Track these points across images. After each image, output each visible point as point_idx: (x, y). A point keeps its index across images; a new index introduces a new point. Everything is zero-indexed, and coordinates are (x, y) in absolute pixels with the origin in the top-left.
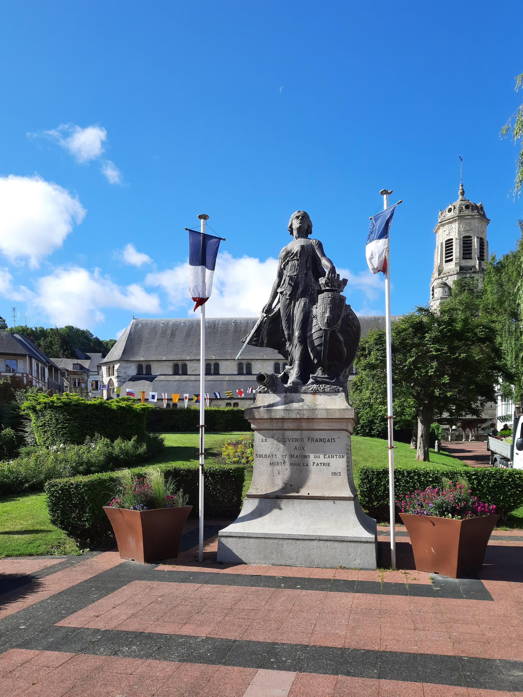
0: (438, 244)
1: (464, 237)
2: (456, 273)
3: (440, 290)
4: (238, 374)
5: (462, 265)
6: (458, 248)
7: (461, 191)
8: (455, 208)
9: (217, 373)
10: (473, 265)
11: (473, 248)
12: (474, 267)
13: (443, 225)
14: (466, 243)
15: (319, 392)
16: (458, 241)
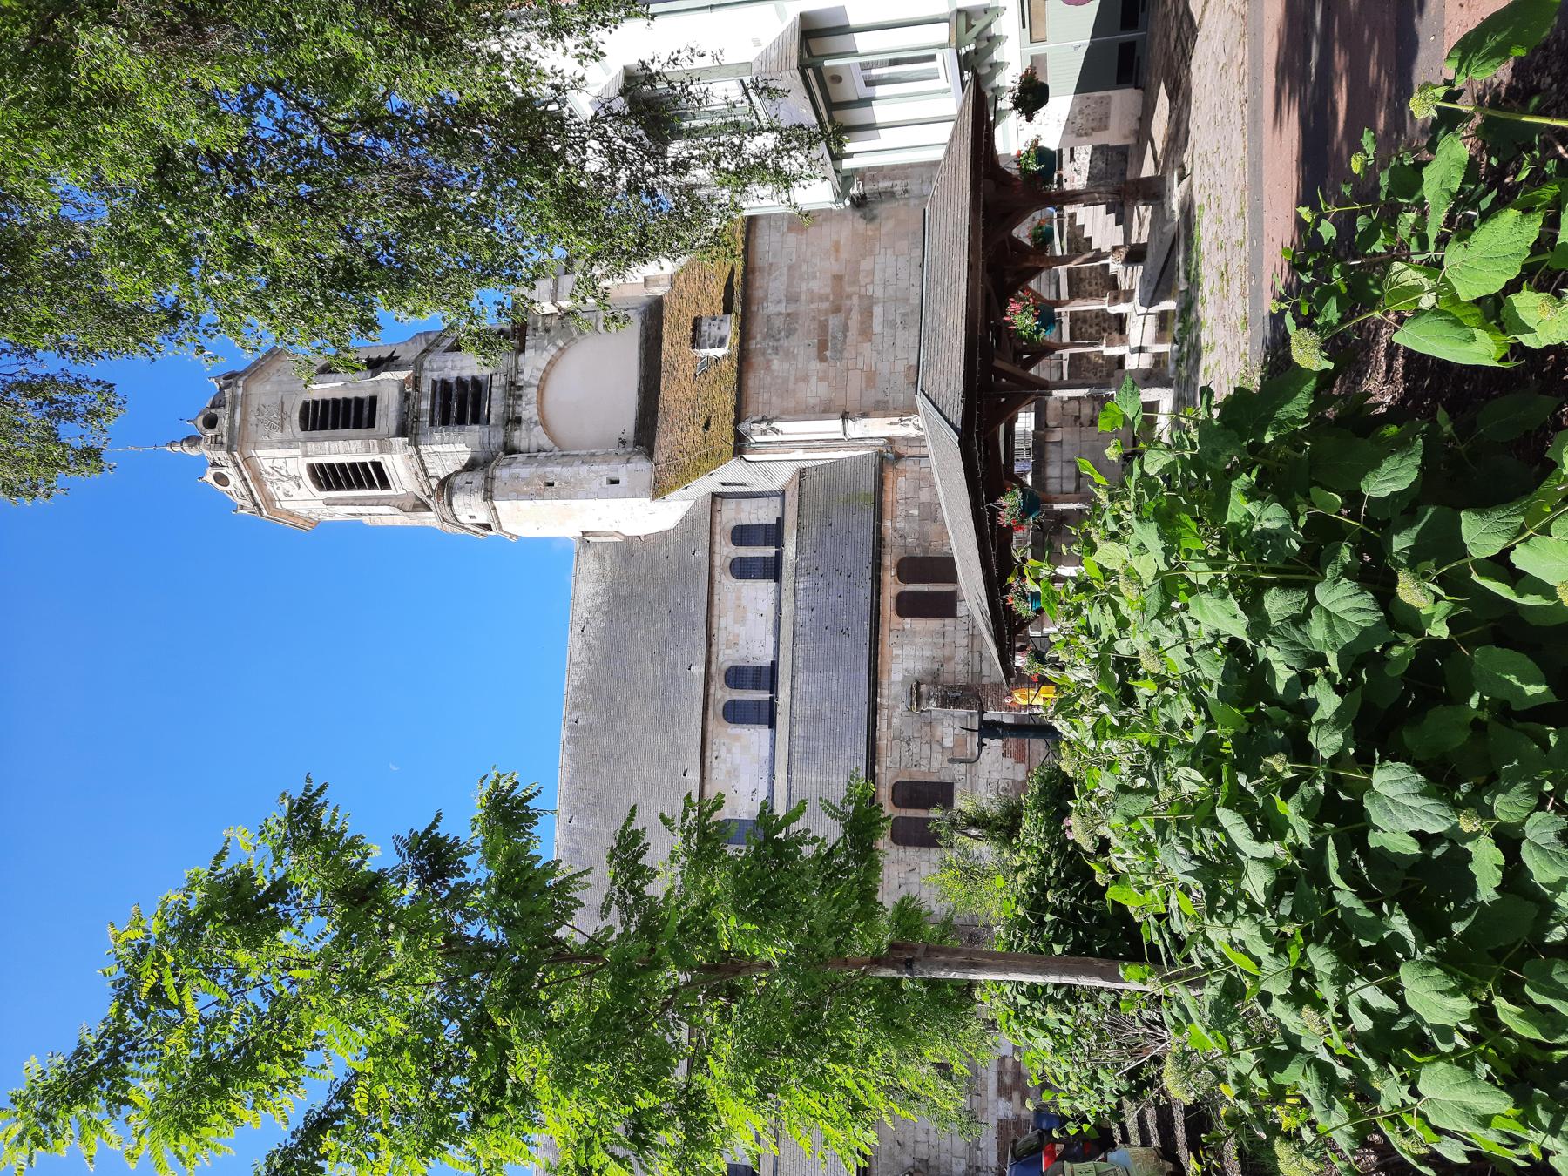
0: (341, 513)
1: (304, 429)
2: (411, 450)
3: (459, 501)
4: (772, 724)
5: (393, 428)
6: (334, 445)
7: (185, 446)
8: (214, 464)
9: (767, 677)
10: (396, 392)
11: (339, 396)
12: (403, 383)
13: (270, 501)
14: (324, 417)
15: (867, 881)
16: (311, 446)
